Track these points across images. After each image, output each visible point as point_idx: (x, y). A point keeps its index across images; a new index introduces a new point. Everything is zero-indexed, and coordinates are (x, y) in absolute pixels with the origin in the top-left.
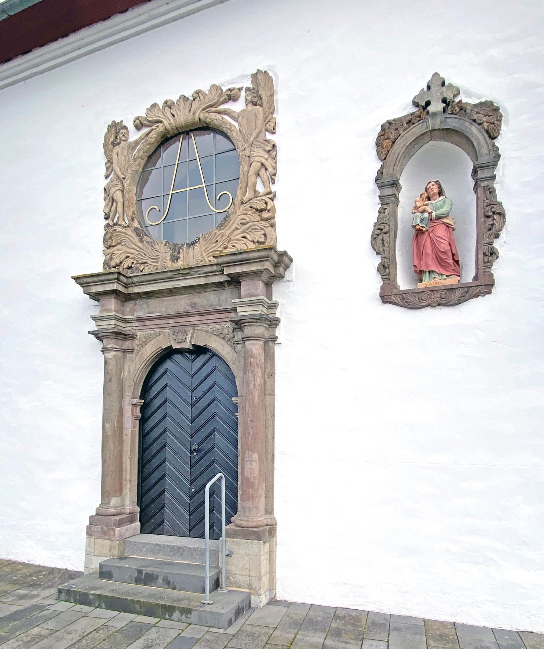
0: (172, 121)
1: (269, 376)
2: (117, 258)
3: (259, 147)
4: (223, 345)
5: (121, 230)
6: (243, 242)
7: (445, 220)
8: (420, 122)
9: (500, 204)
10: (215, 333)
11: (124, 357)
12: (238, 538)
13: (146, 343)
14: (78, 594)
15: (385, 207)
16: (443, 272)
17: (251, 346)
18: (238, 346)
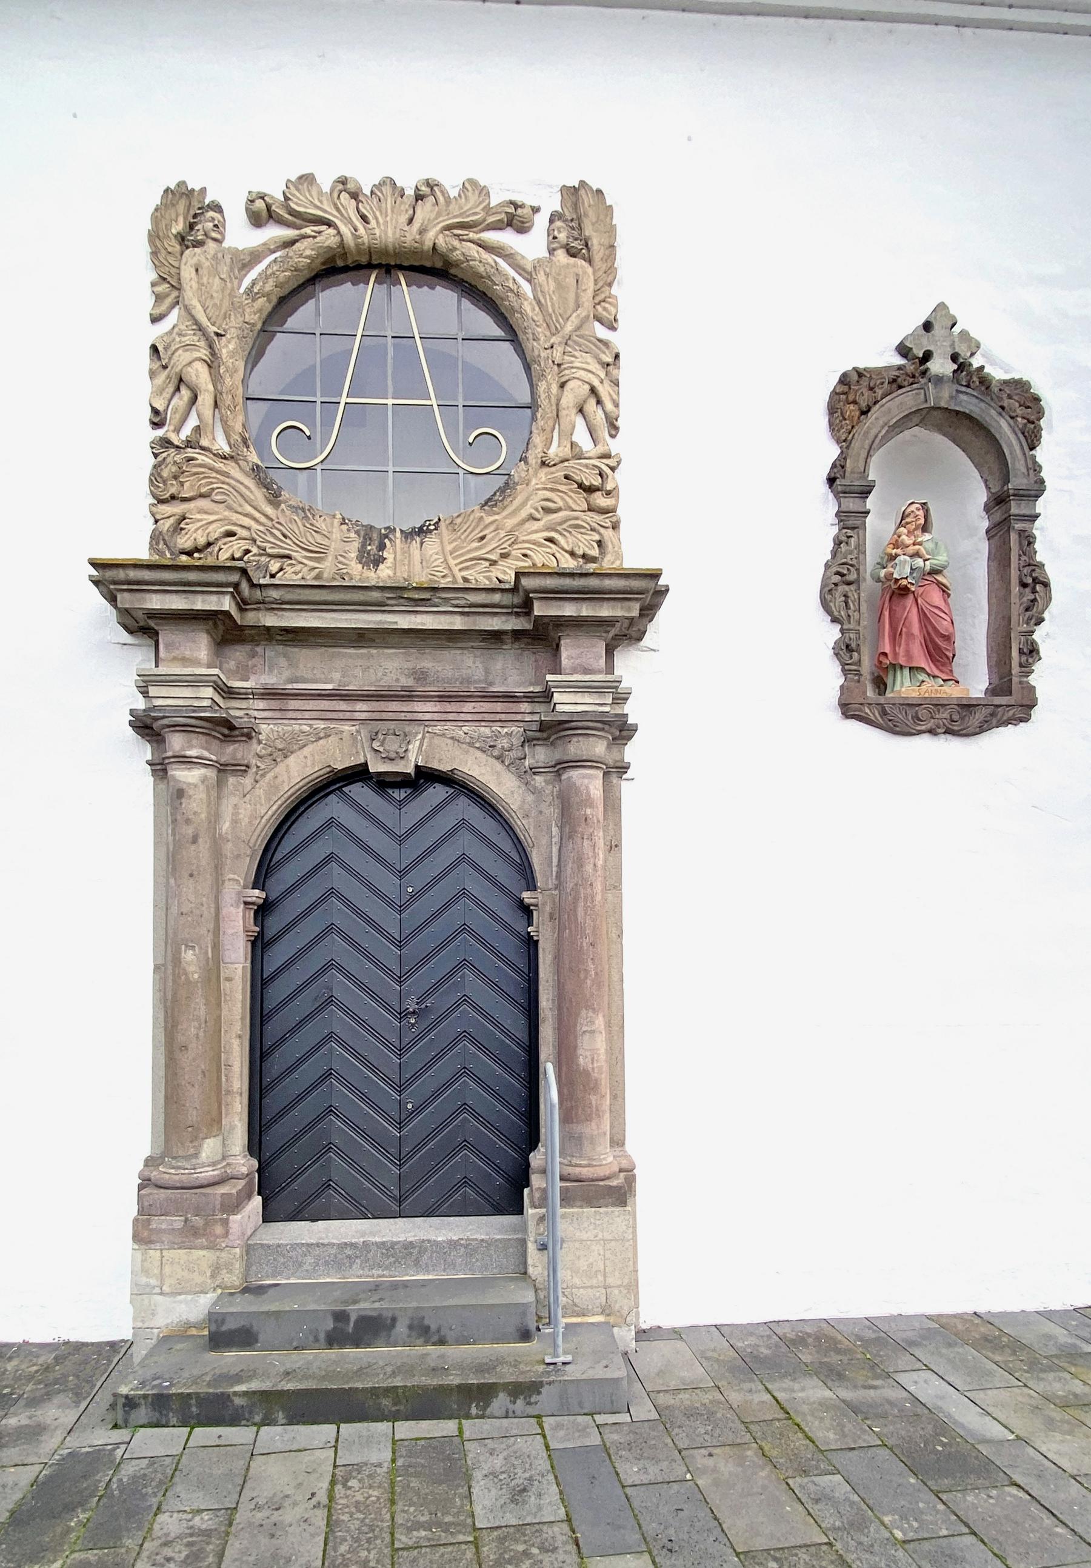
0: (362, 231)
1: (611, 847)
2: (200, 532)
3: (587, 350)
4: (498, 774)
5: (211, 462)
6: (548, 550)
7: (940, 578)
8: (915, 386)
9: (1041, 566)
10: (477, 745)
11: (220, 784)
12: (572, 1207)
13: (286, 753)
14: (193, 1402)
15: (850, 532)
16: (937, 672)
17: (586, 781)
18: (537, 778)
